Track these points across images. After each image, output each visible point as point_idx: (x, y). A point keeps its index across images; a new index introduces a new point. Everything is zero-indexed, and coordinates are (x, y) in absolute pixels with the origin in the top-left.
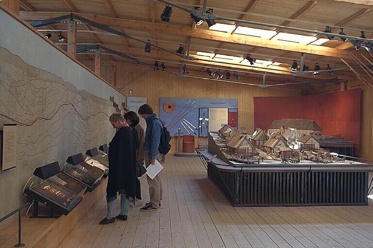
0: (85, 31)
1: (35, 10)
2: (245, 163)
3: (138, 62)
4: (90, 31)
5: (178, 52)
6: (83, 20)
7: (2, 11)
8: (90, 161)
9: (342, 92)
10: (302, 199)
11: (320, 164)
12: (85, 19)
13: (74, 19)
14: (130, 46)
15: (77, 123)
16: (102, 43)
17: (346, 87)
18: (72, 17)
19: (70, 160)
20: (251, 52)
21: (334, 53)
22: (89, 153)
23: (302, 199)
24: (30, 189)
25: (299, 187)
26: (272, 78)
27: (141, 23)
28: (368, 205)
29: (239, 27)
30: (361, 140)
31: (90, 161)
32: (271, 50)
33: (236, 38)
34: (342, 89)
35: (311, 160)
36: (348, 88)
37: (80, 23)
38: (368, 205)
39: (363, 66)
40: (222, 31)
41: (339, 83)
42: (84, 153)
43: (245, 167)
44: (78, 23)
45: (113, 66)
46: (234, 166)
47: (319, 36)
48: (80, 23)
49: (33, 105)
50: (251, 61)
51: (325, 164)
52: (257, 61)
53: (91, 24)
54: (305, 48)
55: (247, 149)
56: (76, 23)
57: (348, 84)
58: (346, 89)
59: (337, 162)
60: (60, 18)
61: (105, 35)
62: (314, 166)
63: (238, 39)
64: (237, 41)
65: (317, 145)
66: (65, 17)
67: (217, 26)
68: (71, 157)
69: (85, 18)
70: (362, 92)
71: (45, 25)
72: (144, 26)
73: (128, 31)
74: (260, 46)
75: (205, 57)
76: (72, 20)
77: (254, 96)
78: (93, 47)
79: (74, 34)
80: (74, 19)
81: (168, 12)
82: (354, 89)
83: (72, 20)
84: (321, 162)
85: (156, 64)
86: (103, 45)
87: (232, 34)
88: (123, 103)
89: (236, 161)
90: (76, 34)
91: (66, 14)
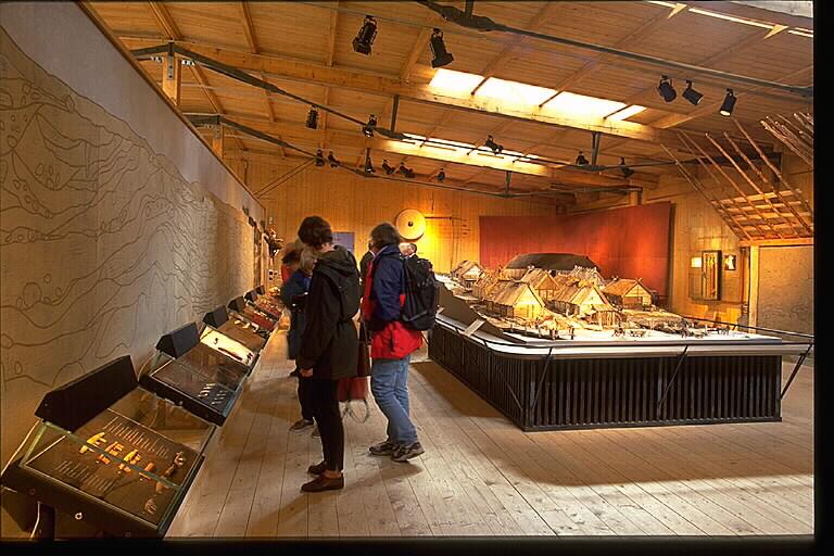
2: (543, 337)
6: (195, 57)
8: (212, 339)
11: (689, 338)
12: (198, 55)
13: (176, 55)
15: (184, 252)
16: (225, 112)
17: (639, 199)
18: (171, 50)
19: (168, 345)
20: (495, 130)
21: (649, 135)
22: (214, 320)
24: (24, 465)
28: (780, 420)
29: (492, 81)
32: (431, 163)
34: (634, 203)
36: (643, 202)
37: (188, 63)
38: (780, 420)
41: (625, 194)
44: (183, 62)
45: (242, 160)
47: (629, 102)
48: (188, 63)
49: (51, 185)
51: (700, 339)
55: (530, 309)
57: (643, 196)
60: (147, 51)
63: (485, 104)
65: (647, 300)
66: (158, 50)
69: (198, 53)
72: (310, 72)
76: (171, 54)
77: (480, 214)
80: (176, 55)
83: (171, 54)
84: (692, 334)
86: (226, 117)
90: (179, 85)
91: (160, 43)
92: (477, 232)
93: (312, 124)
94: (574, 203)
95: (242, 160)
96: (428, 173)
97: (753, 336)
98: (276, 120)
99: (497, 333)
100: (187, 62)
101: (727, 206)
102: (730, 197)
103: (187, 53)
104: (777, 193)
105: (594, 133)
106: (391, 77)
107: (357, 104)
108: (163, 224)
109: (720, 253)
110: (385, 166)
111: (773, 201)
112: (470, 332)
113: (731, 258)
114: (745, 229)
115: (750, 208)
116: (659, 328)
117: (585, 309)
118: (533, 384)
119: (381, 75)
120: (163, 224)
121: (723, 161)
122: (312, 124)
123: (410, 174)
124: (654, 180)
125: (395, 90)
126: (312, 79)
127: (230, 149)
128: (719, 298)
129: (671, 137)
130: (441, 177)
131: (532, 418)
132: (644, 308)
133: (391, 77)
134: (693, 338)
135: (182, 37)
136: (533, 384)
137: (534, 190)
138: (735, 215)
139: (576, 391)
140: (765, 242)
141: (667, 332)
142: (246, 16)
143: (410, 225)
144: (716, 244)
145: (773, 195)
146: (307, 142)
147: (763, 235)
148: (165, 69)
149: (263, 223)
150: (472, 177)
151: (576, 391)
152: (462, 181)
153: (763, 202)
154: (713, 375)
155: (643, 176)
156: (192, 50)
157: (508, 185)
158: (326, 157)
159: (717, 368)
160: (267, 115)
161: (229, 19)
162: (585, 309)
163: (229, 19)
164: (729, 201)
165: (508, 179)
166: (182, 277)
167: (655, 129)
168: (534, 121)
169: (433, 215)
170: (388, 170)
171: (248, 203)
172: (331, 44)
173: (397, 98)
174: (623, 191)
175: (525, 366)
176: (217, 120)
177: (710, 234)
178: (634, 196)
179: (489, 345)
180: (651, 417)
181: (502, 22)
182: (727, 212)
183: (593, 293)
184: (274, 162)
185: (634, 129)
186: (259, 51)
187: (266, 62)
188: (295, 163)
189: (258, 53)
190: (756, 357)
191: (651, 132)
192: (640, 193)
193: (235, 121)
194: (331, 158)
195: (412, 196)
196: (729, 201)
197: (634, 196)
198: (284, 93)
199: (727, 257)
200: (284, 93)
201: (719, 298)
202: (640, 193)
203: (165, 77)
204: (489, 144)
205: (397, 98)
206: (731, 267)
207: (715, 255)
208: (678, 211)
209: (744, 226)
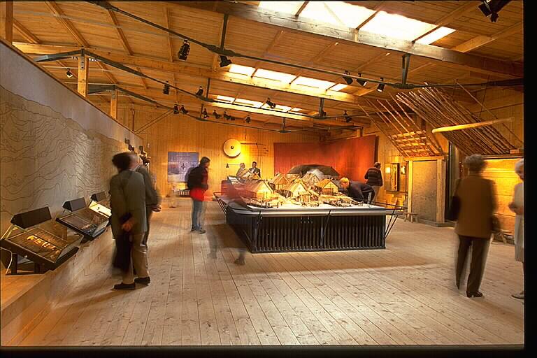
0: (100, 72)
1: (40, 42)
3: (233, 119)
5: (197, 94)
6: (96, 57)
7: (2, 45)
9: (358, 138)
10: (321, 244)
14: (148, 88)
16: (118, 83)
17: (361, 134)
18: (83, 53)
20: (272, 96)
22: (94, 198)
23: (321, 244)
26: (294, 125)
28: (385, 248)
32: (224, 94)
33: (256, 82)
34: (358, 136)
35: (330, 204)
36: (364, 135)
38: (385, 248)
39: (380, 113)
40: (238, 73)
43: (263, 211)
45: (131, 109)
46: (252, 210)
50: (272, 105)
52: (277, 106)
53: (105, 61)
54: (324, 93)
57: (364, 132)
58: (361, 136)
59: (351, 207)
60: (69, 54)
61: (122, 75)
62: (333, 210)
64: (257, 84)
65: (336, 190)
67: (234, 68)
70: (377, 139)
71: (52, 60)
72: (161, 65)
73: (144, 71)
74: (291, 91)
75: (224, 102)
76: (83, 55)
77: (274, 141)
78: (109, 88)
79: (85, 71)
81: (185, 49)
83: (83, 55)
84: (340, 205)
85: (176, 108)
86: (119, 86)
87: (252, 77)
88: (140, 147)
89: (255, 205)
90: (87, 71)
92: (273, 152)
93: (166, 92)
94: (329, 135)
95: (131, 109)
96: (242, 117)
97: (373, 207)
98: (148, 88)
100: (92, 59)
101: (396, 139)
102: (395, 134)
103: (91, 54)
105: (321, 98)
106: (206, 67)
107: (191, 85)
108: (69, 152)
109: (398, 164)
110: (215, 114)
113: (404, 167)
114: (406, 152)
115: (405, 140)
117: (295, 194)
118: (322, 229)
119: (202, 67)
120: (69, 152)
122: (166, 92)
123: (228, 117)
124: (368, 123)
125: (208, 75)
126: (162, 69)
127: (124, 103)
128: (398, 190)
129: (362, 100)
130: (248, 120)
132: (333, 194)
133: (206, 67)
135: (89, 46)
136: (322, 229)
137: (305, 127)
138: (400, 143)
139: (289, 234)
140: (415, 159)
141: (333, 205)
142: (122, 38)
143: (232, 148)
144: (397, 160)
145: (413, 133)
146: (169, 101)
147: (414, 155)
148: (80, 63)
149: (141, 148)
150: (268, 120)
151: (289, 234)
152: (263, 122)
153: (410, 137)
154: (293, 227)
155: (362, 120)
156: (94, 53)
157: (284, 125)
158: (179, 108)
159: (287, 225)
160: (142, 85)
161: (113, 38)
162: (295, 194)
163: (113, 38)
164: (395, 136)
165: (284, 122)
166: (80, 177)
167: (355, 96)
168: (287, 92)
169: (249, 142)
170: (217, 116)
171: (129, 136)
172: (170, 52)
173: (209, 79)
174: (353, 129)
175: (324, 219)
176: (114, 88)
177: (394, 154)
180: (319, 247)
181: (239, 52)
183: (300, 186)
184: (150, 110)
185: (343, 97)
186: (132, 53)
187: (136, 59)
188: (164, 111)
189: (132, 55)
190: (359, 216)
192: (361, 130)
193: (124, 88)
194: (183, 109)
195: (233, 130)
196: (395, 136)
198: (204, 45)
199: (402, 167)
200: (204, 45)
201: (398, 190)
202: (361, 130)
203: (80, 67)
204: (268, 103)
205: (209, 79)
206: (404, 173)
207: (396, 166)
208: (380, 141)
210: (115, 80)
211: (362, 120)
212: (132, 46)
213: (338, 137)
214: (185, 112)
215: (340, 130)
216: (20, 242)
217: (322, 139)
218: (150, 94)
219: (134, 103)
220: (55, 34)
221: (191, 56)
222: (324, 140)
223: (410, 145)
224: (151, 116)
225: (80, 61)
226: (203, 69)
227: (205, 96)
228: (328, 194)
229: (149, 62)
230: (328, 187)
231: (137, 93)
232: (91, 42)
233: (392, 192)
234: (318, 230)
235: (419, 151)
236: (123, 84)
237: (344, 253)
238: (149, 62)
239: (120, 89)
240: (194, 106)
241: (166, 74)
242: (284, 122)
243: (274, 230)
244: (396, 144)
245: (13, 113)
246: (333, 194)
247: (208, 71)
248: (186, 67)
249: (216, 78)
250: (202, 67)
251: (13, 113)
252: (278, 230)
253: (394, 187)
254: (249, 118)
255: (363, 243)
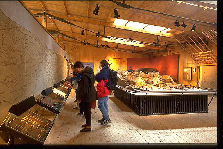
2: (144, 90)
4: (54, 24)
6: (51, 16)
8: (56, 91)
11: (183, 90)
12: (52, 15)
13: (46, 15)
14: (73, 33)
15: (48, 68)
16: (59, 31)
19: (44, 93)
20: (131, 35)
22: (56, 86)
23: (175, 110)
24: (6, 125)
25: (184, 105)
27: (81, 18)
28: (208, 112)
30: (178, 77)
31: (56, 91)
32: (114, 44)
34: (168, 54)
36: (171, 54)
37: (49, 17)
38: (208, 112)
40: (119, 23)
41: (166, 52)
42: (52, 86)
44: (48, 17)
45: (64, 43)
47: (167, 27)
48: (49, 17)
55: (141, 82)
56: (47, 17)
57: (171, 52)
60: (38, 14)
65: (172, 80)
66: (41, 14)
68: (44, 90)
70: (179, 56)
73: (72, 22)
76: (45, 15)
80: (46, 15)
82: (174, 54)
83: (45, 15)
84: (184, 89)
85: (85, 42)
86: (59, 32)
90: (47, 23)
92: (127, 62)
93: (82, 34)
98: (73, 33)
99: (132, 89)
101: (193, 55)
102: (194, 53)
104: (207, 52)
105: (158, 36)
107: (94, 28)
109: (192, 68)
111: (206, 54)
112: (125, 89)
113: (195, 69)
114: (198, 61)
115: (200, 56)
116: (175, 88)
117: (156, 83)
119: (101, 21)
121: (192, 43)
122: (82, 34)
123: (109, 47)
124: (174, 48)
125: (104, 24)
126: (82, 21)
128: (191, 80)
129: (178, 37)
130: (117, 47)
131: (142, 112)
132: (172, 82)
134: (185, 90)
135: (47, 11)
138: (195, 57)
140: (204, 65)
144: (190, 65)
146: (81, 38)
147: (203, 63)
149: (69, 60)
150: (125, 48)
153: (203, 54)
155: (171, 47)
157: (135, 50)
158: (86, 42)
160: (70, 31)
162: (156, 83)
164: (194, 54)
165: (135, 48)
167: (174, 34)
168: (142, 33)
173: (105, 26)
174: (166, 51)
176: (57, 33)
177: (189, 63)
178: (168, 52)
179: (130, 93)
180: (173, 111)
182: (193, 57)
183: (158, 78)
184: (72, 44)
185: (168, 35)
187: (70, 17)
188: (78, 44)
189: (68, 15)
191: (173, 35)
192: (170, 52)
194: (87, 42)
195: (109, 53)
196: (194, 54)
197: (168, 52)
199: (193, 69)
201: (191, 80)
202: (170, 52)
205: (105, 26)
206: (195, 71)
207: (190, 68)
208: (180, 57)
209: (198, 60)
210: (58, 29)
211: (171, 47)
212: (69, 10)
213: (157, 55)
214: (89, 44)
215: (158, 52)
216: (15, 126)
217: (149, 56)
218: (74, 35)
219: (65, 40)
220: (32, 4)
221: (99, 12)
222: (150, 57)
223: (202, 58)
224: (72, 46)
225: (43, 18)
226: (102, 21)
227: (103, 35)
228: (168, 83)
229: (76, 18)
230: (168, 79)
231: (68, 35)
232: (49, 8)
233: (188, 81)
234: (174, 103)
235: (206, 61)
236: (61, 31)
237: (183, 115)
238: (76, 18)
239: (60, 33)
240: (92, 42)
241: (84, 24)
242: (135, 48)
243: (151, 103)
244: (193, 58)
245: (10, 30)
246: (172, 82)
247: (104, 22)
248: (94, 20)
249: (109, 26)
250: (101, 21)
251: (10, 30)
252: (153, 103)
253: (189, 78)
254: (117, 47)
255: (197, 109)
